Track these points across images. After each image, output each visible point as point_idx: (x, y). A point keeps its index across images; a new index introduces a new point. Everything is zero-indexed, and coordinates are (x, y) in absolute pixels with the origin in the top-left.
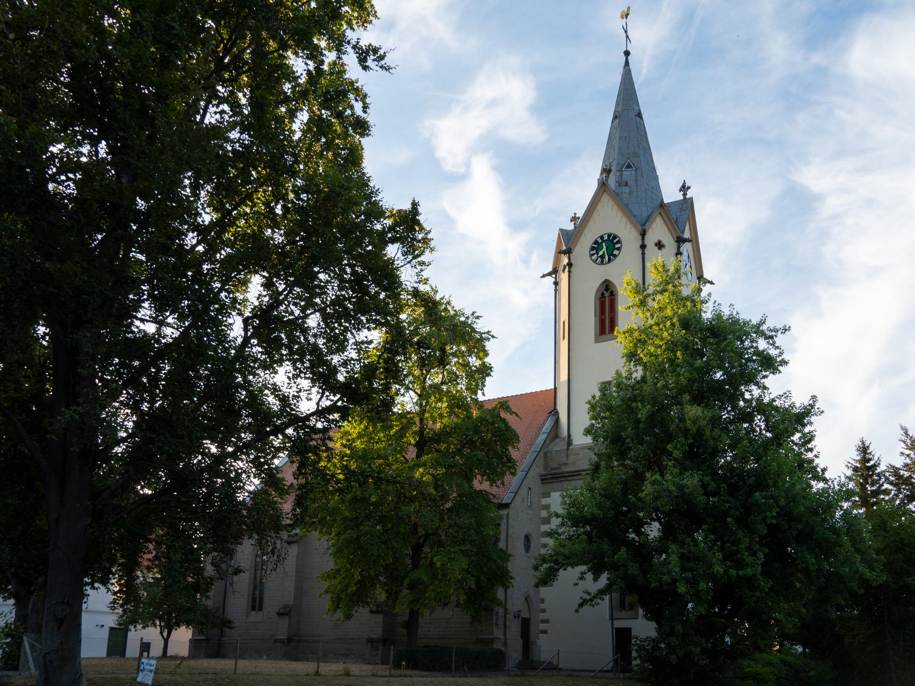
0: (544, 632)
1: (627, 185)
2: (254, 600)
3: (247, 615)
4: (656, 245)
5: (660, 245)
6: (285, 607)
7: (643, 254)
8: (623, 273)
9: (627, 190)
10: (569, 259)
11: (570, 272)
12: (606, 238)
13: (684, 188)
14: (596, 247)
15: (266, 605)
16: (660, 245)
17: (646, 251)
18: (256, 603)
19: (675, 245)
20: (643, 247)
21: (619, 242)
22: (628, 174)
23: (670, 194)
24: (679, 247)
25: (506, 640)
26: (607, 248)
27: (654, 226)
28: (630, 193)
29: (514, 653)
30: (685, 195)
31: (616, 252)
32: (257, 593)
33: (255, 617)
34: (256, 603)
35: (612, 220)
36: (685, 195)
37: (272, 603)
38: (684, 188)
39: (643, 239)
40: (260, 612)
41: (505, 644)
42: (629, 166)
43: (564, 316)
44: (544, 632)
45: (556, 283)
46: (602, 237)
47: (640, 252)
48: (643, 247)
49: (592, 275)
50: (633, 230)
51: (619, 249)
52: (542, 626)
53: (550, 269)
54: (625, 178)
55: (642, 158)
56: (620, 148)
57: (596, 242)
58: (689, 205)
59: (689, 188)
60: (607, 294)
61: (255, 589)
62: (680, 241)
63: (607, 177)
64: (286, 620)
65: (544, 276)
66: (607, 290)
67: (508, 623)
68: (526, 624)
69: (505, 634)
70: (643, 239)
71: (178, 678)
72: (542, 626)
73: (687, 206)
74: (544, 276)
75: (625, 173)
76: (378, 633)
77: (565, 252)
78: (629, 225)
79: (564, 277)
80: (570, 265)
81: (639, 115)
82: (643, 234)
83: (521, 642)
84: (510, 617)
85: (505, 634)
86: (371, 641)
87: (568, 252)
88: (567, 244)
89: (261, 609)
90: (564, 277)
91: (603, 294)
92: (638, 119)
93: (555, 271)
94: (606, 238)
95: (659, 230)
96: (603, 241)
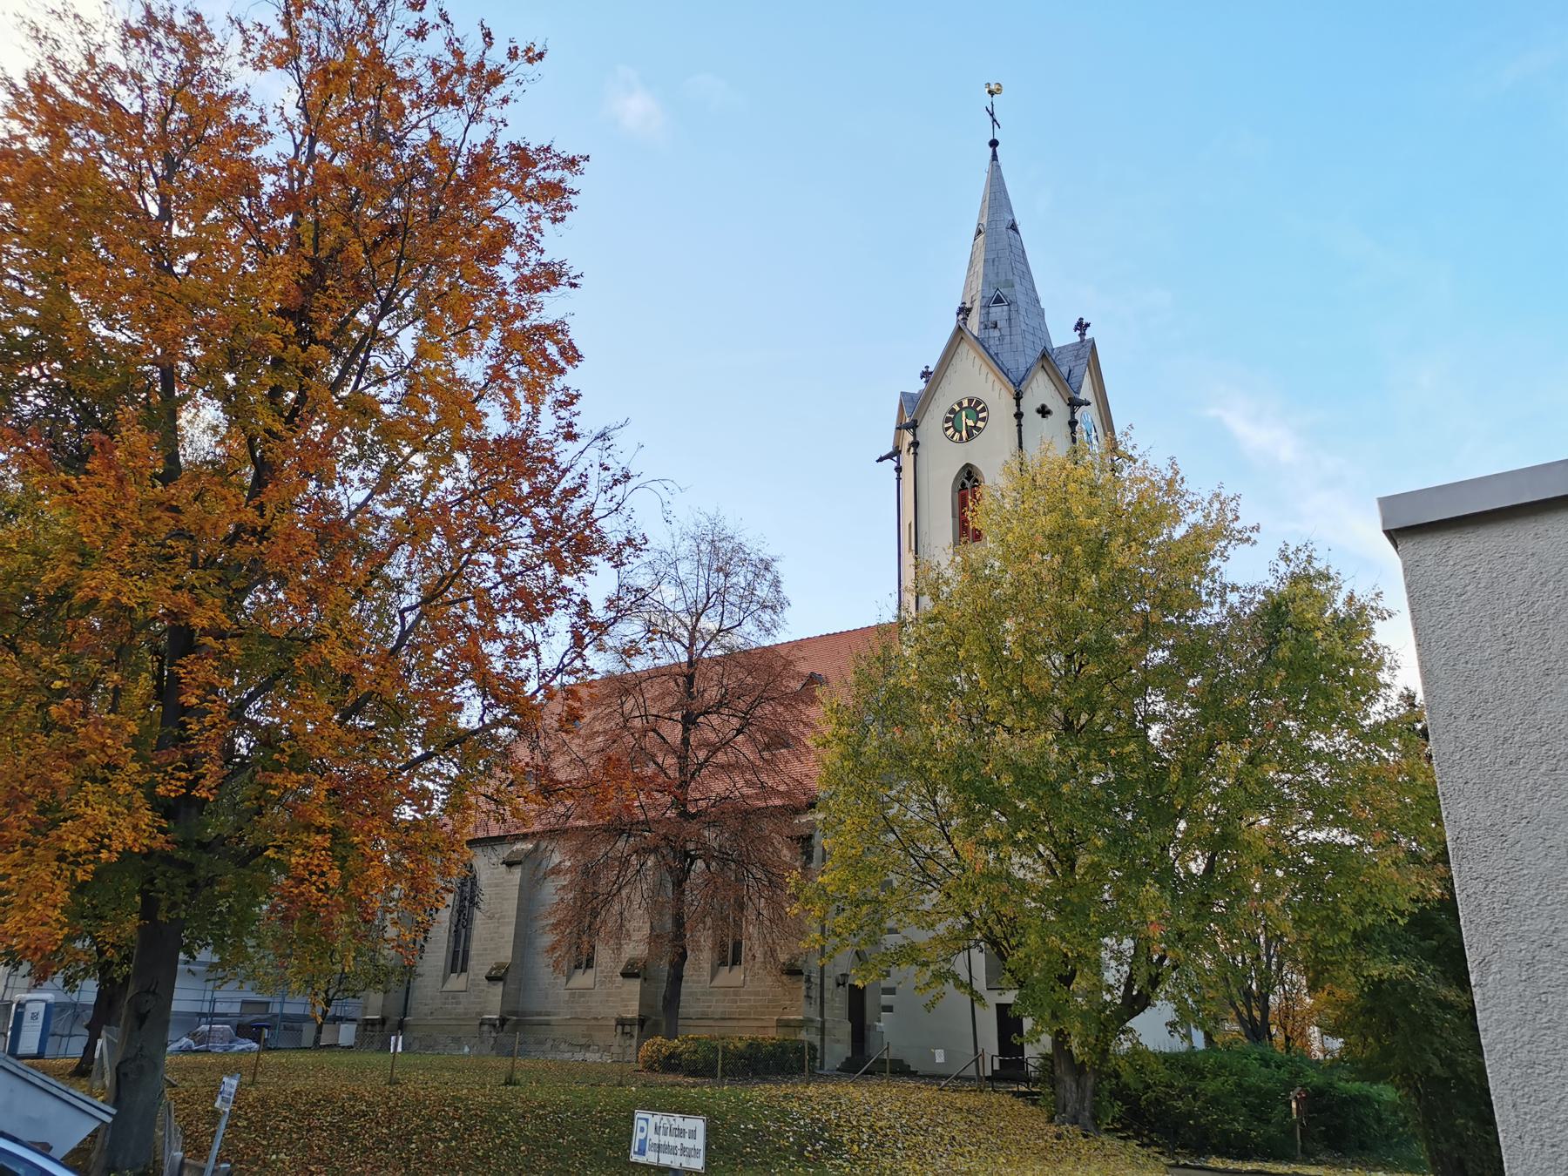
0: (889, 1009)
1: (996, 326)
2: (455, 953)
3: (445, 979)
4: (1038, 411)
5: (1044, 412)
6: (499, 967)
7: (1019, 425)
8: (992, 454)
9: (996, 333)
10: (914, 435)
11: (915, 454)
12: (965, 404)
13: (1081, 326)
14: (952, 418)
15: (472, 963)
16: (1044, 412)
17: (1023, 421)
18: (458, 960)
19: (1068, 409)
20: (1019, 415)
21: (983, 410)
22: (998, 312)
23: (1061, 336)
24: (1073, 413)
25: (823, 1023)
26: (968, 419)
27: (1034, 384)
28: (1001, 338)
29: (839, 1049)
30: (1082, 335)
31: (980, 424)
32: (467, 889)
33: (457, 982)
34: (458, 960)
35: (975, 378)
36: (1082, 335)
37: (480, 965)
38: (1081, 326)
39: (1018, 405)
40: (464, 975)
41: (822, 1030)
42: (998, 300)
43: (908, 517)
44: (889, 1009)
45: (899, 469)
46: (960, 404)
47: (1015, 422)
48: (1019, 415)
49: (943, 460)
50: (1004, 392)
51: (983, 419)
52: (886, 999)
53: (890, 449)
54: (993, 317)
55: (1017, 287)
56: (985, 275)
57: (952, 411)
58: (1089, 349)
59: (1088, 325)
60: (968, 485)
61: (457, 942)
62: (1074, 404)
63: (965, 319)
64: (498, 988)
65: (881, 460)
66: (969, 479)
67: (827, 995)
68: (857, 998)
69: (822, 1015)
70: (1018, 405)
71: (592, 1057)
72: (886, 999)
73: (1087, 353)
74: (881, 460)
75: (993, 310)
76: (632, 1010)
77: (907, 428)
78: (998, 385)
79: (907, 460)
80: (915, 444)
81: (1014, 227)
82: (1018, 397)
83: (847, 1027)
84: (830, 983)
85: (822, 1015)
86: (622, 1022)
87: (913, 426)
88: (911, 418)
89: (464, 970)
90: (907, 460)
91: (963, 484)
92: (1011, 232)
93: (896, 453)
94: (965, 404)
95: (1041, 390)
96: (962, 409)
